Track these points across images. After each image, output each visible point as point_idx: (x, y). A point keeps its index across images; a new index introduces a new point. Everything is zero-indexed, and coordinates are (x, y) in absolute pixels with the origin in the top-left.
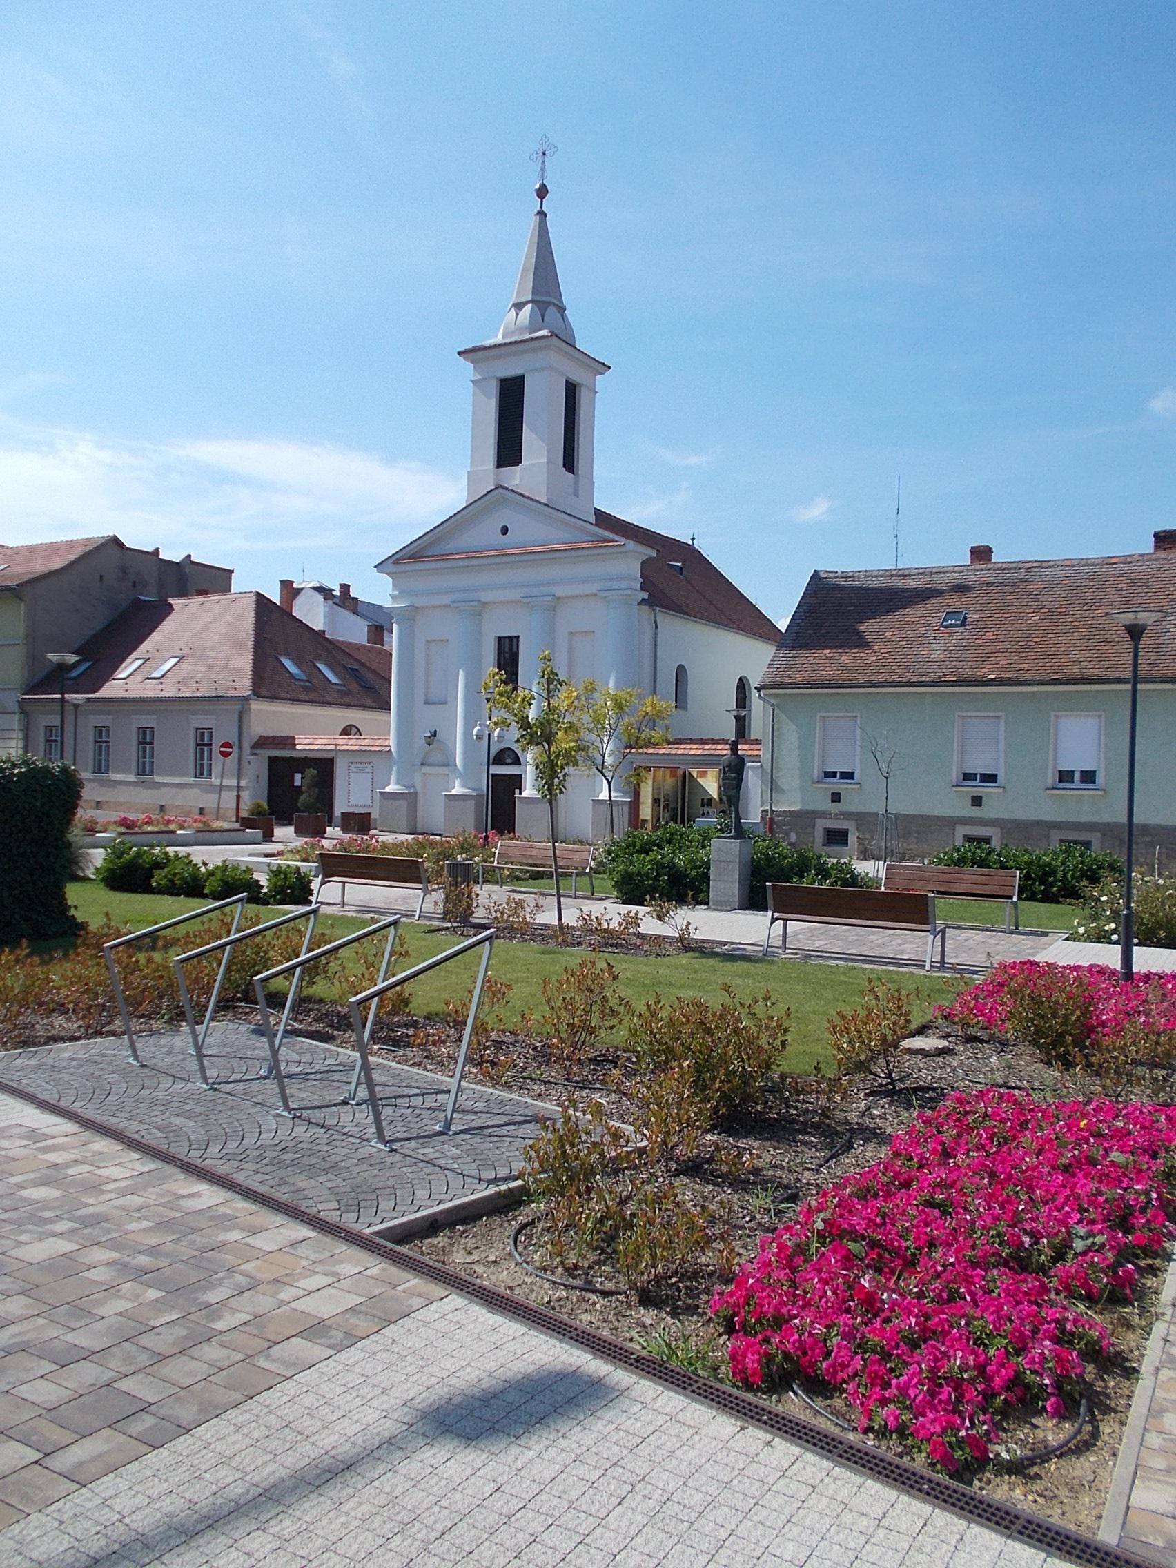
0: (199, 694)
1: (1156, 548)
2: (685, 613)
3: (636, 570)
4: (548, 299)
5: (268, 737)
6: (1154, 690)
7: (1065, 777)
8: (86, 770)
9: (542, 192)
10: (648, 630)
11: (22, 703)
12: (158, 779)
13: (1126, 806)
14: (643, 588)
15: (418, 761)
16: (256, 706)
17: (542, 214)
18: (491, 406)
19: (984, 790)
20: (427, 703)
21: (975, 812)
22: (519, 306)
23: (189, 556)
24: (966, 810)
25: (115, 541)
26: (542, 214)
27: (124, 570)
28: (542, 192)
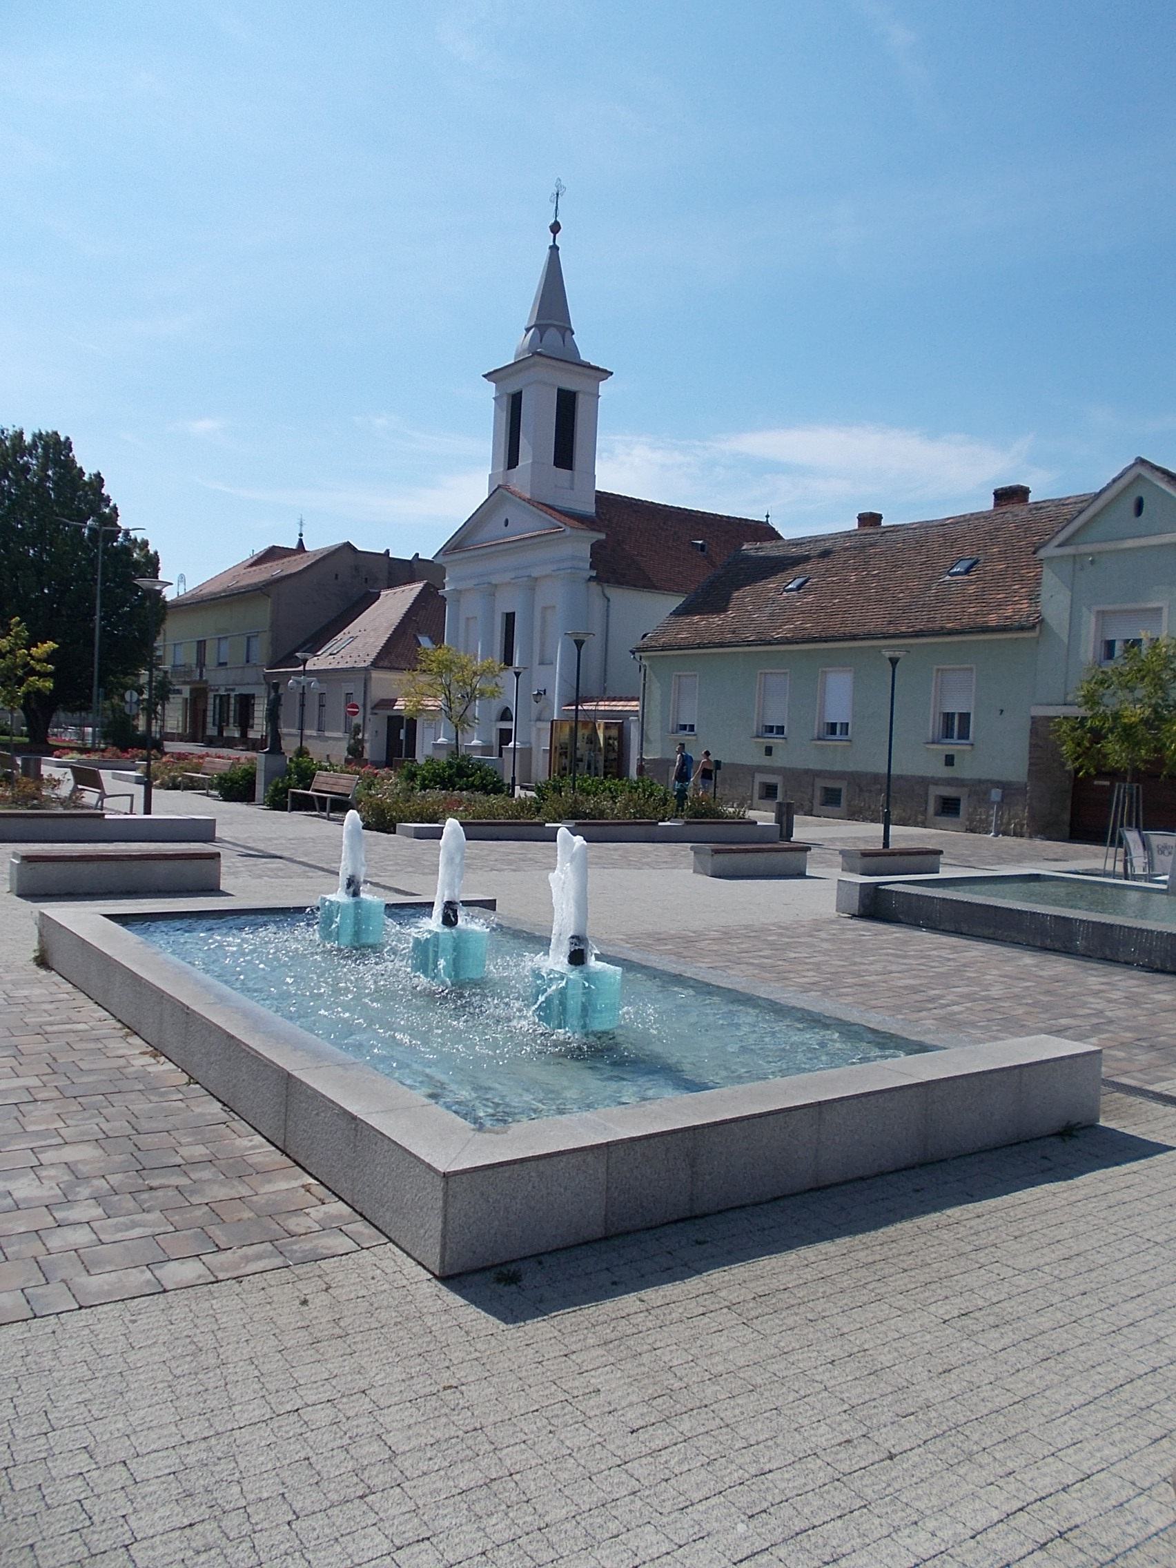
0: (339, 666)
1: (996, 505)
2: (656, 588)
3: (587, 552)
4: (549, 322)
5: (383, 700)
6: (851, 648)
7: (832, 728)
8: (311, 728)
9: (555, 228)
10: (598, 603)
11: (266, 676)
12: (327, 734)
13: (21, 820)
14: (592, 567)
15: (534, 717)
16: (376, 674)
17: (554, 249)
18: (504, 417)
19: (775, 741)
20: (541, 663)
21: (766, 761)
22: (528, 330)
23: (417, 555)
24: (760, 759)
25: (348, 545)
26: (554, 249)
27: (357, 569)
28: (555, 228)
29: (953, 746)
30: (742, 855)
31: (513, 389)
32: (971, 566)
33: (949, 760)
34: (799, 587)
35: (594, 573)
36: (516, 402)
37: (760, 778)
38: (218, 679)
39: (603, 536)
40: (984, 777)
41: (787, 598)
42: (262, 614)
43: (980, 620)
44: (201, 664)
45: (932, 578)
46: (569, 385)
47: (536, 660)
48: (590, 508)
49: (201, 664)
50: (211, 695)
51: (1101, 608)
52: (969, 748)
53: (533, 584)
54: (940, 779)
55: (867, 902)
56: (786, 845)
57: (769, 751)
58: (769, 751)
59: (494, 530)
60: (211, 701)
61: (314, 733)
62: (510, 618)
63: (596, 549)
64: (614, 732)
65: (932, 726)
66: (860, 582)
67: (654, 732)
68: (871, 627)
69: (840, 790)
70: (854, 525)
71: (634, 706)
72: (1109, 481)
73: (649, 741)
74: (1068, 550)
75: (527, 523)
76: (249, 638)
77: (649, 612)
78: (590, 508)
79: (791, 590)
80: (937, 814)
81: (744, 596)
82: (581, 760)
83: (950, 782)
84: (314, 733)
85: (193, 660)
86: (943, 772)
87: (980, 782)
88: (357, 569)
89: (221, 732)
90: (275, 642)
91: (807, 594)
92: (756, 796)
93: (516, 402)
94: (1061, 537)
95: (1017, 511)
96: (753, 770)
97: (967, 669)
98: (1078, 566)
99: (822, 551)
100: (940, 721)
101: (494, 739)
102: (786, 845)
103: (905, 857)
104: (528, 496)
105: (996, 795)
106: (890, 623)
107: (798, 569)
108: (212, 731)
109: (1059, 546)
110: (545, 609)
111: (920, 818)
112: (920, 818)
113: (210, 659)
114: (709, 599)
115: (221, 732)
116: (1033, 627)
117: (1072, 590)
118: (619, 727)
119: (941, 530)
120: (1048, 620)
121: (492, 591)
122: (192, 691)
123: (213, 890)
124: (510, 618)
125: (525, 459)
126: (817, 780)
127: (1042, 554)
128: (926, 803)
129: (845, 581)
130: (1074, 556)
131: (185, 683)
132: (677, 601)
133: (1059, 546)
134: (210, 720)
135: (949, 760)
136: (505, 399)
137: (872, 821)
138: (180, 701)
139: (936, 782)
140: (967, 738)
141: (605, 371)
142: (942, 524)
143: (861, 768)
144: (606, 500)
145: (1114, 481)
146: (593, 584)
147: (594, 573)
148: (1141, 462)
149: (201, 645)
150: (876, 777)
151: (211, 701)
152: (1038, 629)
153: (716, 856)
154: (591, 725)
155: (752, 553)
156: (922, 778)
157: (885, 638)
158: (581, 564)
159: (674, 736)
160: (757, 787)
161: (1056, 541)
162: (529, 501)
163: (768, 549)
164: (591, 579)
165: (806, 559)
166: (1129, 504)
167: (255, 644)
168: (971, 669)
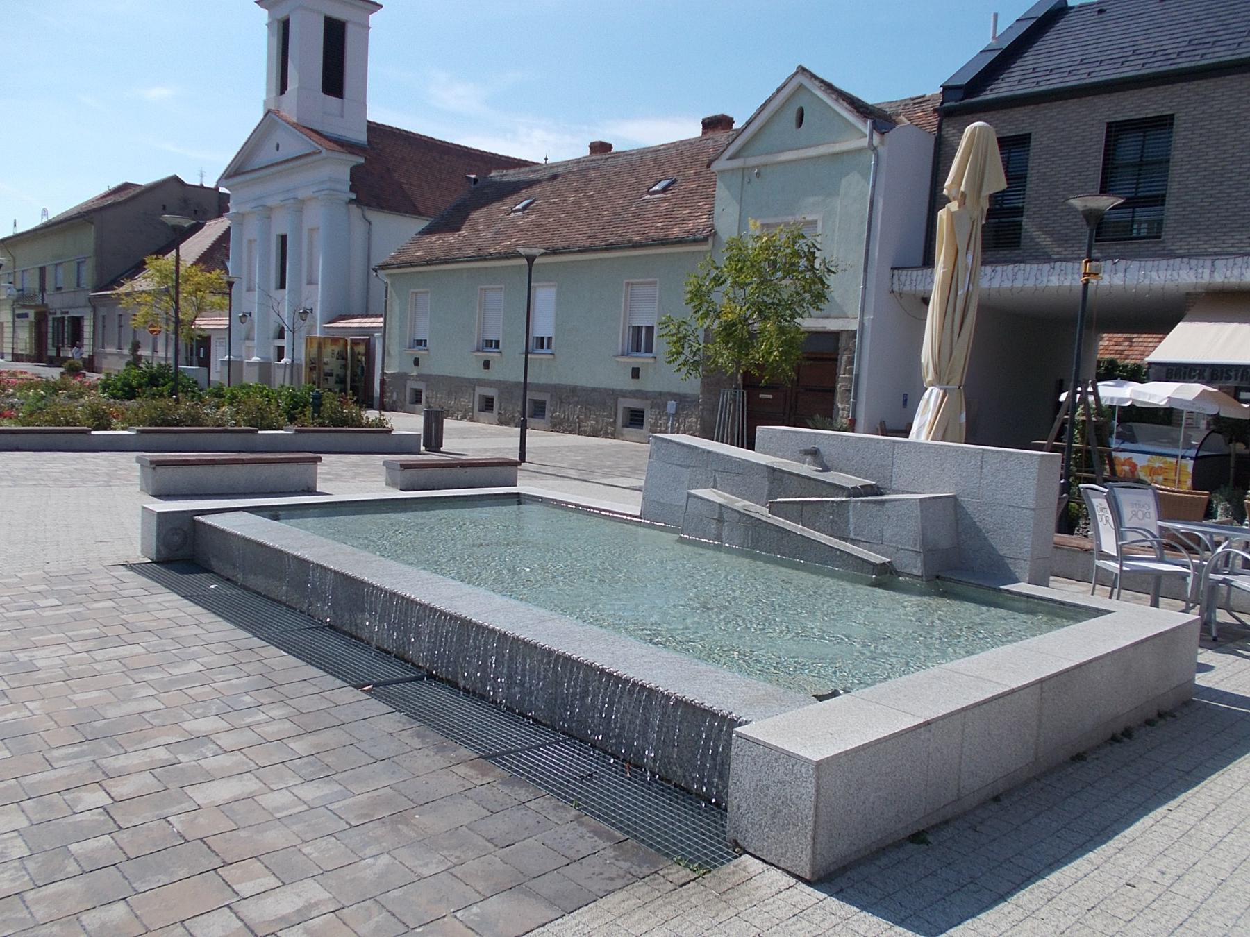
6: (556, 263)
10: (359, 228)
11: (91, 299)
14: (352, 189)
18: (275, 42)
19: (492, 355)
24: (481, 374)
27: (185, 201)
29: (641, 359)
30: (209, 468)
31: (281, 15)
32: (668, 186)
33: (636, 373)
34: (525, 208)
35: (354, 196)
36: (285, 26)
37: (480, 391)
38: (55, 303)
39: (362, 161)
40: (666, 389)
41: (514, 218)
42: (87, 240)
43: (663, 233)
44: (43, 289)
45: (636, 197)
46: (338, 13)
47: (304, 281)
48: (362, 137)
49: (43, 289)
50: (50, 318)
51: (766, 221)
52: (652, 361)
53: (299, 206)
54: (627, 391)
55: (176, 539)
56: (433, 457)
57: (487, 365)
58: (487, 365)
59: (267, 155)
60: (50, 324)
61: (114, 350)
62: (284, 238)
63: (355, 172)
64: (361, 349)
65: (621, 338)
66: (578, 202)
67: (394, 348)
68: (572, 242)
69: (544, 403)
70: (587, 152)
71: (378, 322)
72: (774, 91)
73: (389, 354)
74: (737, 163)
75: (293, 144)
76: (79, 264)
77: (397, 233)
78: (362, 137)
79: (518, 211)
80: (625, 426)
81: (479, 216)
82: (331, 375)
83: (636, 394)
84: (114, 350)
85: (37, 286)
86: (631, 385)
87: (661, 394)
88: (185, 201)
89: (58, 353)
90: (100, 268)
91: (528, 214)
92: (476, 408)
93: (285, 26)
94: (732, 150)
95: (721, 136)
96: (473, 383)
97: (650, 283)
98: (746, 179)
99: (554, 175)
100: (629, 334)
101: (272, 354)
102: (433, 457)
103: (468, 469)
104: (295, 120)
105: (671, 406)
106: (589, 238)
107: (530, 191)
108: (52, 352)
109: (730, 158)
110: (311, 230)
111: (610, 429)
112: (610, 429)
113: (49, 286)
114: (450, 221)
115: (58, 353)
116: (706, 239)
117: (741, 202)
118: (366, 340)
119: (654, 155)
120: (720, 234)
121: (267, 213)
122: (37, 314)
123: (311, 491)
124: (284, 238)
125: (292, 84)
126: (621, 400)
127: (716, 167)
128: (616, 414)
129: (564, 201)
130: (743, 169)
131: (30, 307)
132: (423, 224)
133: (730, 158)
134: (50, 341)
135: (636, 373)
136: (275, 25)
137: (570, 433)
138: (27, 324)
139: (624, 394)
140: (651, 352)
141: (375, 4)
142: (656, 150)
143: (564, 381)
144: (374, 128)
145: (779, 90)
146: (353, 207)
147: (354, 196)
148: (802, 70)
149: (42, 269)
150: (517, 384)
151: (50, 324)
152: (710, 240)
153: (160, 470)
154: (342, 342)
155: (498, 179)
156: (613, 390)
157: (581, 252)
158: (339, 187)
159: (410, 352)
160: (477, 399)
161: (732, 150)
162: (293, 125)
163: (512, 175)
164: (351, 201)
165: (536, 182)
166: (792, 115)
167: (84, 268)
168: (655, 283)
